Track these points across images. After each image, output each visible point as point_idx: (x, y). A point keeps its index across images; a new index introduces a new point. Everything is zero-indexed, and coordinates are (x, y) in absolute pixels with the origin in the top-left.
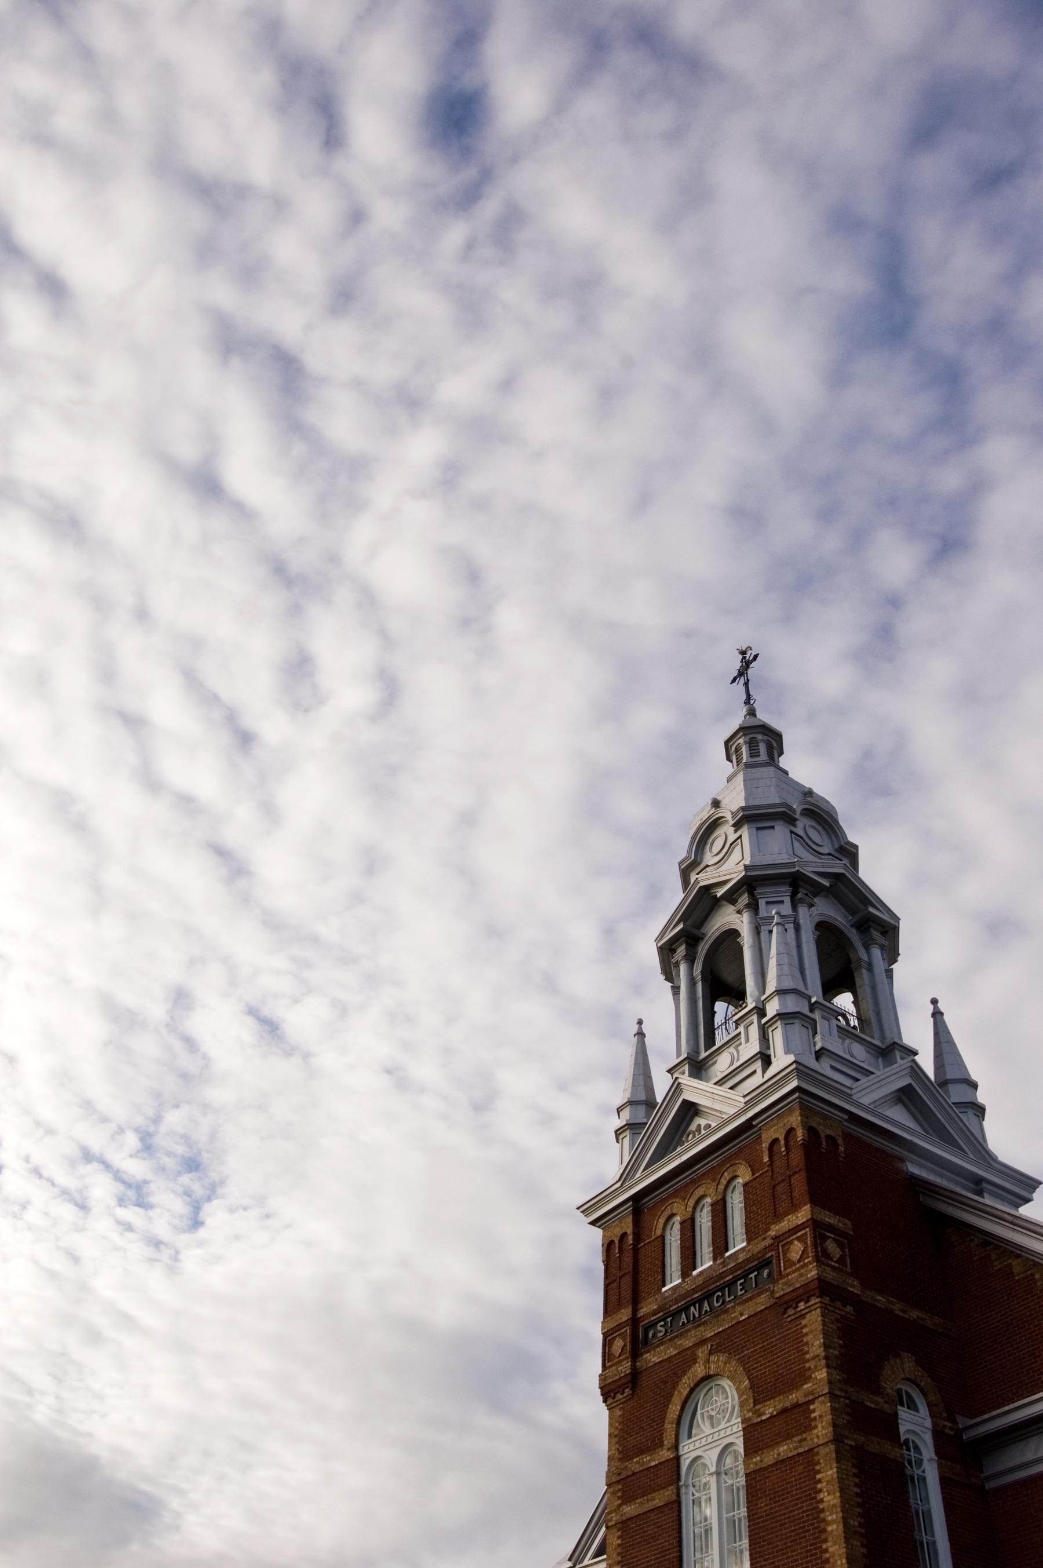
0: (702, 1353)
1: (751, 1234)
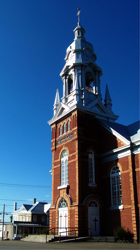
0: (64, 146)
1: (70, 130)
